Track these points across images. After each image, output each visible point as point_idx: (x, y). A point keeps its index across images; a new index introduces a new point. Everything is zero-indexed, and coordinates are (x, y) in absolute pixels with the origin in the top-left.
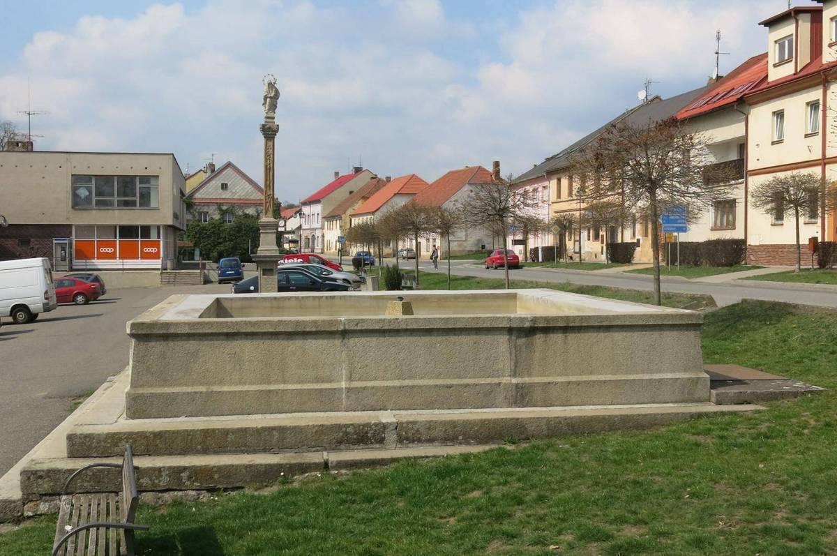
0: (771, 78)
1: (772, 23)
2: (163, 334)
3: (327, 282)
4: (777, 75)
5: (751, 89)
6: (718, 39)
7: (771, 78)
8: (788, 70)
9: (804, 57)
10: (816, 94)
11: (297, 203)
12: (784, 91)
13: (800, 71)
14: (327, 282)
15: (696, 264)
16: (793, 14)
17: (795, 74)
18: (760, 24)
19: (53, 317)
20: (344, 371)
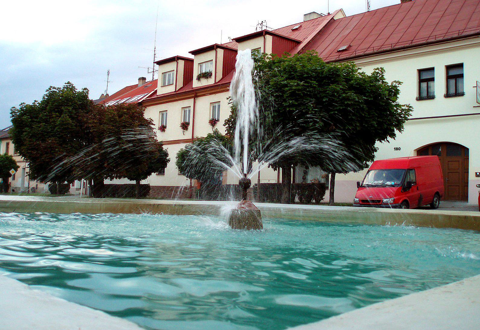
0: (159, 93)
1: (160, 63)
2: (209, 277)
3: (292, 170)
4: (161, 91)
5: (147, 98)
6: (108, 75)
7: (159, 93)
8: (171, 89)
9: (180, 84)
10: (189, 103)
11: (224, 40)
12: (214, 91)
13: (179, 90)
14: (292, 170)
15: (56, 193)
16: (215, 48)
17: (175, 92)
18: (189, 52)
19: (76, 285)
20: (90, 269)
